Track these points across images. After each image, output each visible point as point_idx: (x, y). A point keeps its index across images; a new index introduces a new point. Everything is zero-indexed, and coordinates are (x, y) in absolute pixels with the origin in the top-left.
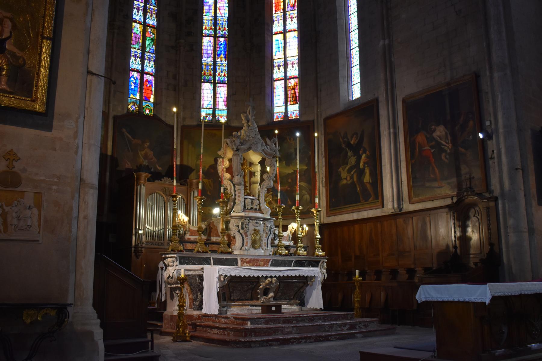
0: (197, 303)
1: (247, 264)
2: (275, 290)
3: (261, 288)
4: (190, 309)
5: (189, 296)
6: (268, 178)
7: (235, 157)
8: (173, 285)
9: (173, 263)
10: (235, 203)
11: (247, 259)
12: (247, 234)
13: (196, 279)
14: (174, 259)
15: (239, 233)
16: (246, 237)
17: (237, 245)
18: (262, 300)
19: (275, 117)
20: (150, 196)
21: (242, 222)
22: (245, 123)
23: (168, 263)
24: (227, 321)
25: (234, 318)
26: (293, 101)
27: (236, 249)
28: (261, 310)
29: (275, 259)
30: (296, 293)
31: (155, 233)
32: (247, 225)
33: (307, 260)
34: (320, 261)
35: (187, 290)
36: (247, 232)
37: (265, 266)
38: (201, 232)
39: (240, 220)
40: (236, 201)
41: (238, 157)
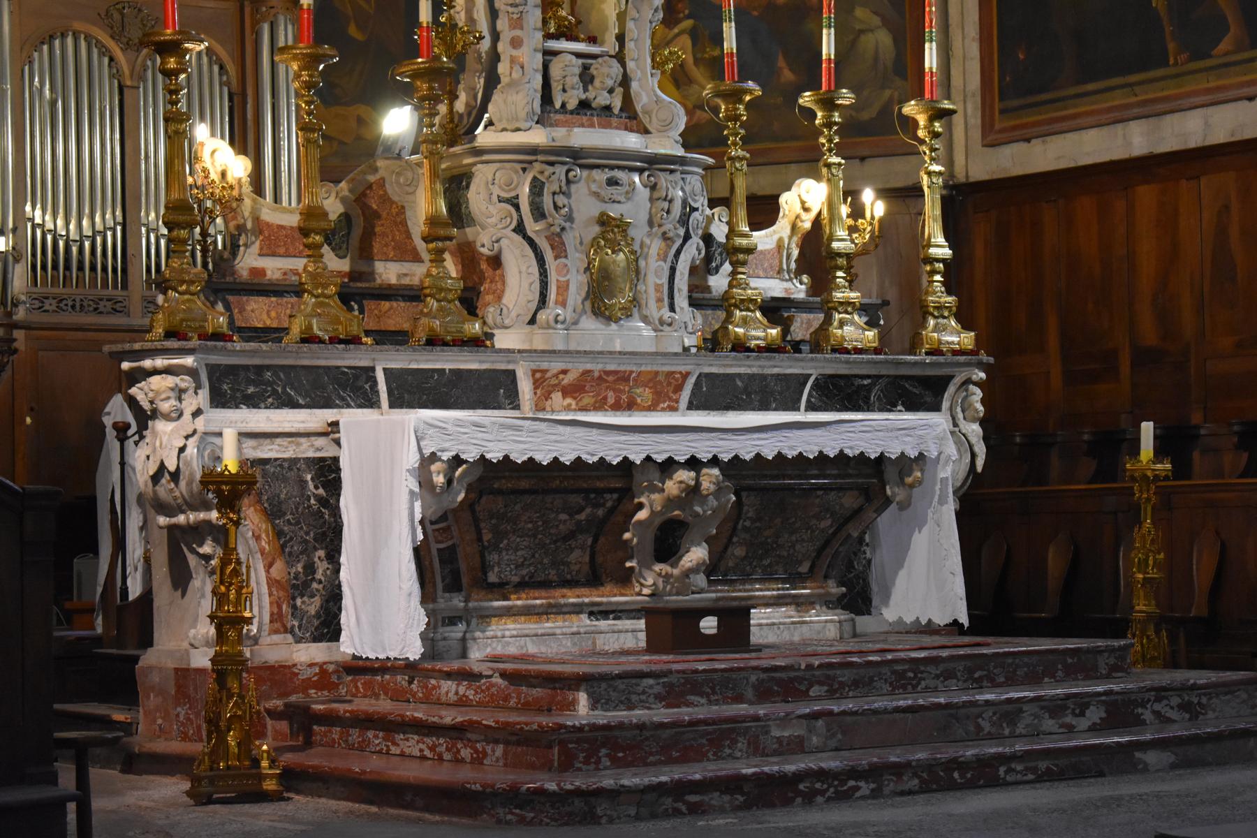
0: (312, 606)
1: (568, 401)
3: (640, 522)
5: (269, 567)
8: (183, 512)
9: (180, 399)
11: (565, 372)
12: (563, 244)
14: (185, 381)
15: (518, 238)
16: (556, 258)
17: (509, 299)
18: (650, 581)
20: (41, 52)
21: (535, 179)
23: (152, 402)
24: (470, 694)
25: (504, 675)
27: (507, 322)
29: (714, 370)
30: (827, 543)
31: (75, 249)
32: (563, 193)
33: (881, 377)
34: (948, 379)
35: (257, 538)
36: (563, 229)
37: (663, 410)
38: (317, 238)
39: (524, 170)
40: (502, 68)
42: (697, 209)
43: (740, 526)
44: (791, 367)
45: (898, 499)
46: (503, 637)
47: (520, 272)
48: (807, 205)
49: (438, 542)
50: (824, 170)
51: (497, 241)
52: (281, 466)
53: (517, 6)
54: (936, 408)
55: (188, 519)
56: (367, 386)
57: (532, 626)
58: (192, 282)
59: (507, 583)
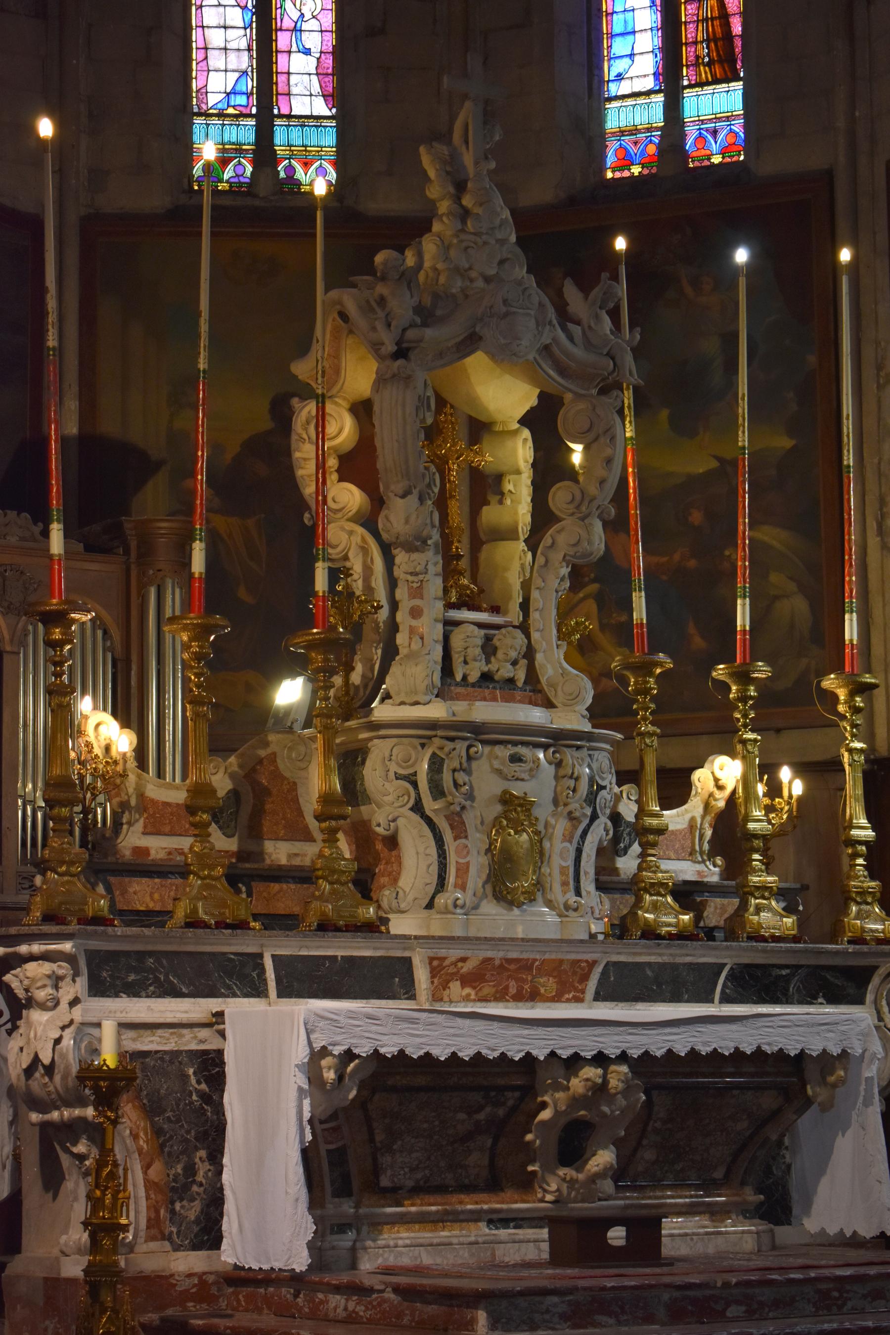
0: (192, 1211)
1: (467, 990)
2: (623, 1133)
3: (543, 1123)
4: (153, 1245)
9: (56, 987)
11: (464, 960)
13: (185, 1077)
14: (61, 969)
15: (416, 818)
17: (405, 882)
18: (554, 1187)
19: (611, 158)
21: (434, 755)
23: (27, 990)
24: (360, 1309)
26: (709, 64)
27: (403, 906)
28: (545, 1246)
29: (622, 958)
32: (464, 770)
33: (798, 967)
35: (135, 1137)
36: (463, 808)
39: (423, 746)
40: (401, 639)
42: (604, 788)
43: (650, 1128)
44: (704, 956)
45: (819, 1100)
46: (396, 1246)
47: (417, 853)
48: (720, 783)
49: (328, 1142)
50: (739, 747)
51: (394, 820)
52: (162, 1059)
53: (416, 574)
54: (859, 1001)
55: (62, 1115)
56: (254, 974)
57: (426, 1235)
58: (71, 863)
59: (400, 1188)
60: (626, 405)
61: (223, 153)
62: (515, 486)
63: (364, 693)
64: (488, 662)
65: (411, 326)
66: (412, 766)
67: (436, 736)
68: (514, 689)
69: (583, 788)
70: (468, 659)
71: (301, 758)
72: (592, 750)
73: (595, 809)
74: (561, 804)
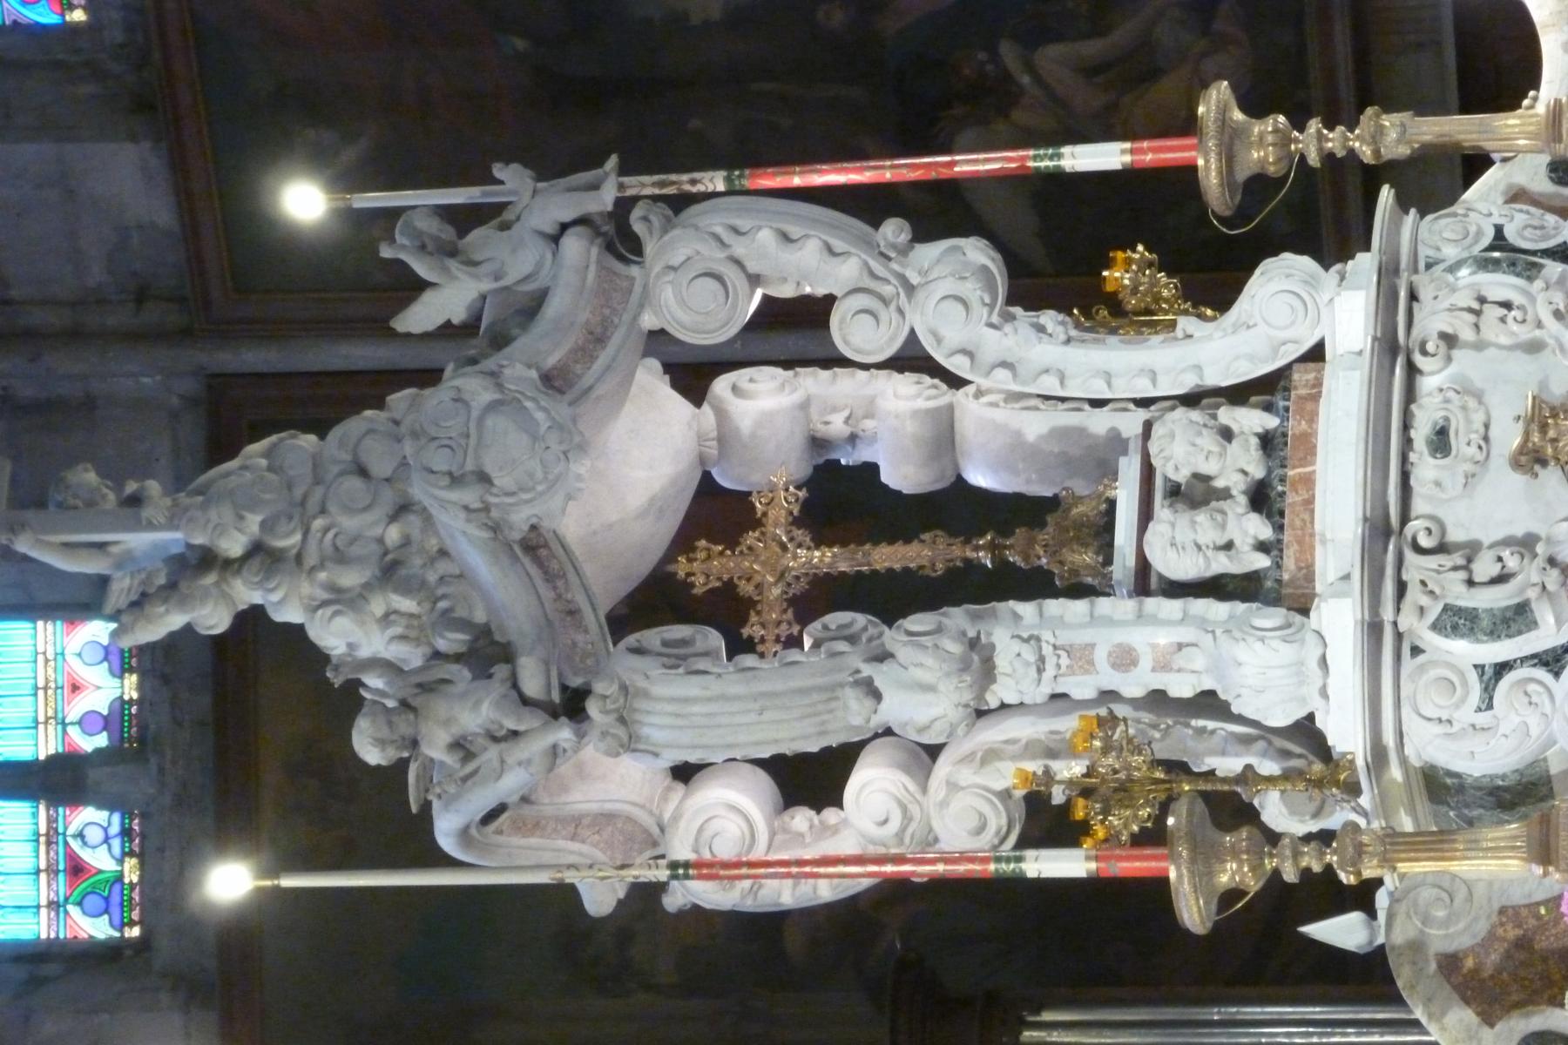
6: (885, 302)
7: (657, 726)
10: (1209, 703)
21: (1436, 627)
22: (227, 598)
32: (1470, 560)
36: (1552, 561)
39: (1416, 651)
40: (1182, 687)
41: (658, 690)
42: (1499, 230)
53: (1042, 659)
60: (657, 191)
61: (57, 872)
62: (835, 410)
63: (1300, 756)
64: (1225, 494)
65: (515, 686)
66: (1462, 675)
67: (1395, 624)
68: (1285, 435)
69: (1500, 285)
70: (1221, 541)
71: (1445, 896)
72: (1416, 261)
73: (1548, 253)
74: (1538, 333)
